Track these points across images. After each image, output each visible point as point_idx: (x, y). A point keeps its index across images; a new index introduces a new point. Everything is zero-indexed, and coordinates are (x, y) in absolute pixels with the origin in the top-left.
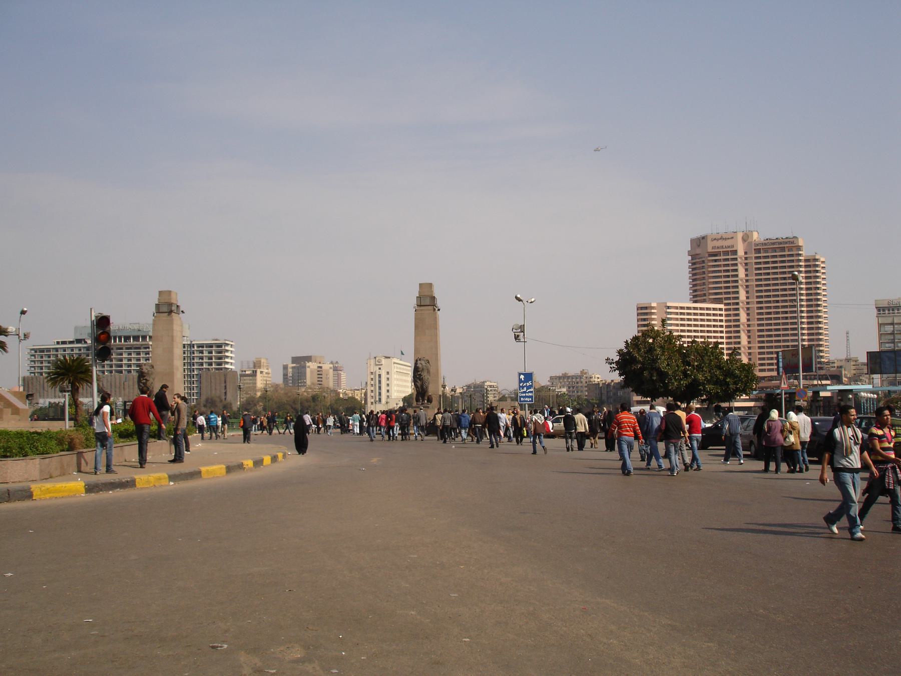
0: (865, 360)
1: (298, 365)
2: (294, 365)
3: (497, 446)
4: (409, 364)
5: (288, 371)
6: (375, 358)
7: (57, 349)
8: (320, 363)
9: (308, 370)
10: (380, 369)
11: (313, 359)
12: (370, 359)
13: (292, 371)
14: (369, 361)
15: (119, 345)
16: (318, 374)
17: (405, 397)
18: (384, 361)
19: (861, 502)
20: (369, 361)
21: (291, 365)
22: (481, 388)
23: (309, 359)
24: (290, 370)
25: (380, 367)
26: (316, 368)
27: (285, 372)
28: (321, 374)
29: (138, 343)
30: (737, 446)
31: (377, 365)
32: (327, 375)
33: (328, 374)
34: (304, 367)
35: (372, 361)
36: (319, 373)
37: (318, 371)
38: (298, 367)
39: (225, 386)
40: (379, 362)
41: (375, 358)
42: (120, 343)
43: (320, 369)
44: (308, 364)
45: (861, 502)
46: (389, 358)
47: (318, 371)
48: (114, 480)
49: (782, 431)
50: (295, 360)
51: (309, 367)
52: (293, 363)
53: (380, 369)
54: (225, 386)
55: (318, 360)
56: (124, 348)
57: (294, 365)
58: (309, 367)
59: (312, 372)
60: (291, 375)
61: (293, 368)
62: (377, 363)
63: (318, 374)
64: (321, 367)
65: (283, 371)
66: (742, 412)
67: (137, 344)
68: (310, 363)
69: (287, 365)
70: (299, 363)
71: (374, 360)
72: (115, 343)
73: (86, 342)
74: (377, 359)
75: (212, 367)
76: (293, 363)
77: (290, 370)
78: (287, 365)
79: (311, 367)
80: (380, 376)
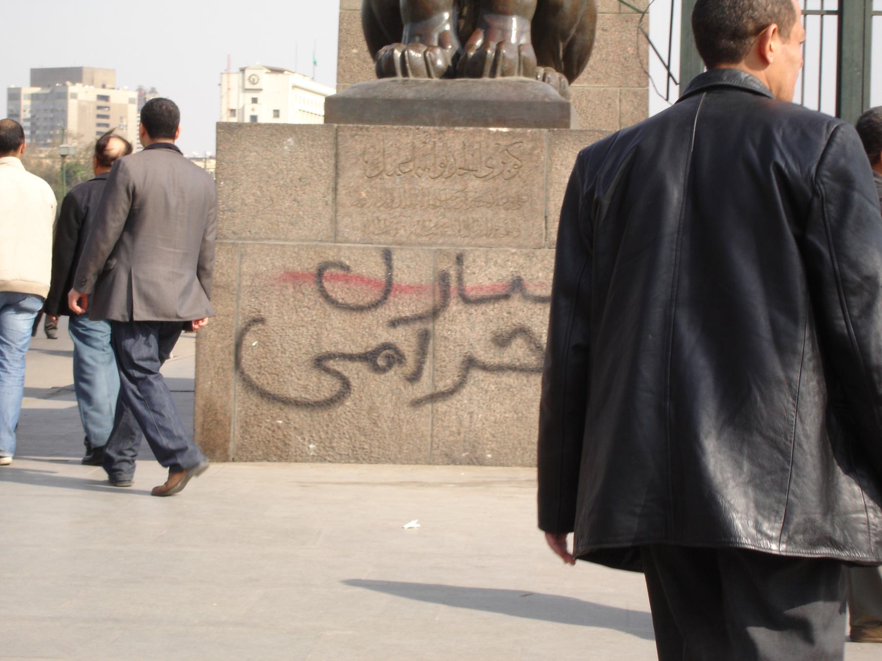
1: (47, 91)
2: (37, 90)
3: (417, 403)
5: (19, 105)
6: (243, 70)
8: (104, 87)
9: (73, 107)
10: (255, 100)
11: (86, 76)
12: (229, 74)
13: (32, 106)
14: (225, 76)
16: (99, 116)
18: (267, 81)
19: (144, 185)
20: (225, 76)
21: (28, 90)
23: (75, 74)
24: (26, 103)
25: (255, 95)
26: (93, 98)
27: (12, 107)
28: (107, 117)
31: (246, 90)
33: (126, 117)
34: (63, 96)
35: (235, 79)
36: (100, 112)
37: (99, 108)
38: (46, 95)
40: (254, 83)
41: (243, 70)
43: (102, 103)
44: (72, 89)
45: (144, 185)
46: (280, 71)
49: (528, 320)
50: (40, 76)
51: (74, 96)
52: (34, 83)
53: (255, 100)
55: (99, 78)
57: (37, 90)
58: (74, 96)
59: (82, 109)
60: (28, 116)
61: (34, 97)
62: (248, 85)
63: (99, 116)
64: (105, 98)
65: (8, 105)
66: (546, 341)
68: (78, 85)
69: (19, 89)
70: (49, 86)
71: (241, 75)
74: (248, 73)
76: (34, 83)
77: (26, 103)
78: (19, 89)
79: (81, 97)
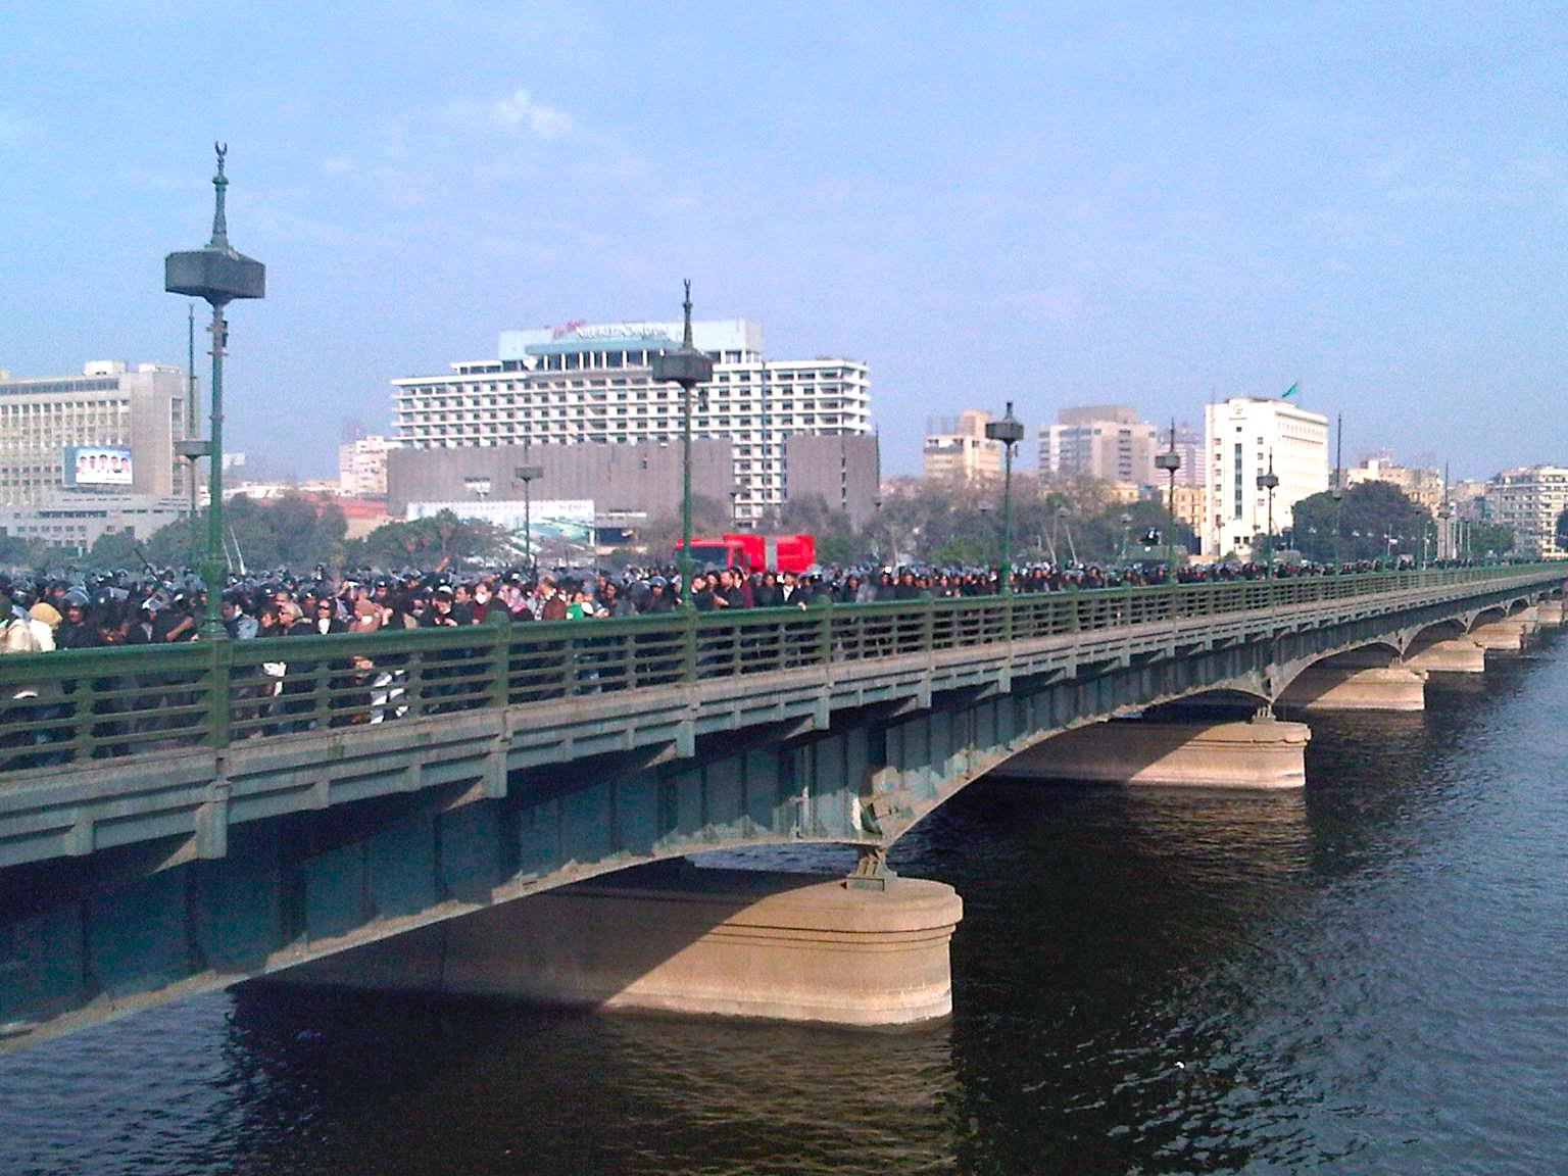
0: (343, 474)
4: (1324, 419)
7: (459, 387)
15: (596, 374)
17: (1299, 503)
22: (1530, 481)
26: (1116, 434)
29: (639, 368)
30: (524, 817)
32: (1143, 451)
36: (1122, 446)
39: (139, 511)
42: (599, 370)
43: (1124, 437)
47: (1122, 442)
48: (615, 696)
54: (139, 511)
55: (1122, 414)
56: (629, 380)
59: (1105, 444)
61: (1062, 434)
67: (637, 372)
72: (587, 370)
73: (525, 368)
75: (813, 426)
80: (1238, 447)
